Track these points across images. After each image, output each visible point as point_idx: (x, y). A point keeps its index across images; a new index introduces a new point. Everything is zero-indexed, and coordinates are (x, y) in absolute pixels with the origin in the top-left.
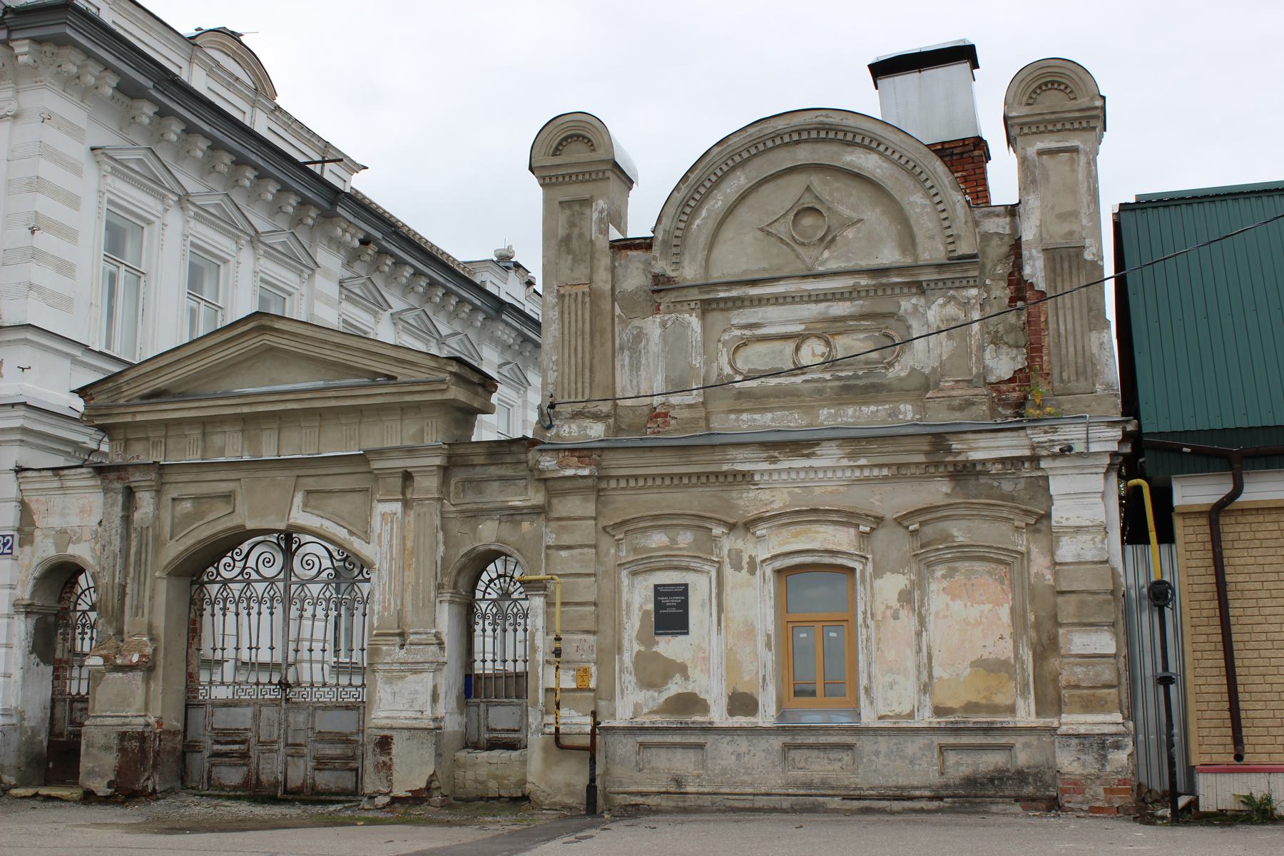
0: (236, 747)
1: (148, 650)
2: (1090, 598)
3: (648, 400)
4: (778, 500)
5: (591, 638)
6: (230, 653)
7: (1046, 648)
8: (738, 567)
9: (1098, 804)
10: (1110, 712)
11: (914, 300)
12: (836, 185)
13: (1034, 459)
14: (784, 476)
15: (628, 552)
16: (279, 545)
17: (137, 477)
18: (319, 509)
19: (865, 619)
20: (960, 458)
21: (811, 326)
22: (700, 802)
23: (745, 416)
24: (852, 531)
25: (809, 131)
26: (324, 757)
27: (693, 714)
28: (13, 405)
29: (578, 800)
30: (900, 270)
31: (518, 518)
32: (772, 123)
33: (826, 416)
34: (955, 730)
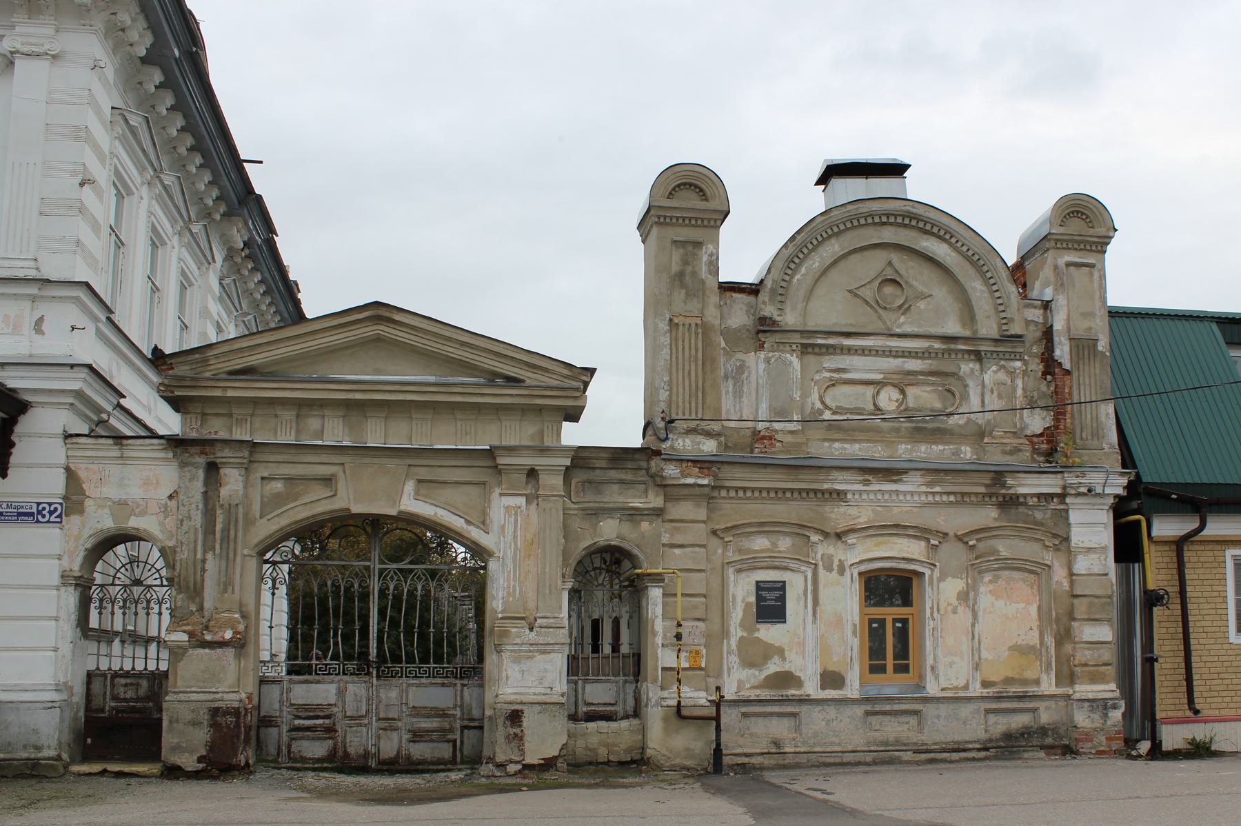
1: (241, 627)
2: (1096, 601)
3: (750, 424)
4: (863, 516)
7: (1064, 636)
8: (829, 569)
9: (1102, 749)
10: (1108, 683)
11: (971, 365)
12: (911, 264)
13: (1062, 497)
14: (872, 496)
17: (227, 452)
19: (932, 614)
20: (1011, 491)
22: (797, 760)
23: (837, 445)
24: (923, 543)
25: (896, 216)
27: (789, 688)
28: (72, 366)
29: (708, 762)
30: (965, 339)
31: (638, 518)
32: (868, 204)
33: (903, 450)
34: (998, 698)
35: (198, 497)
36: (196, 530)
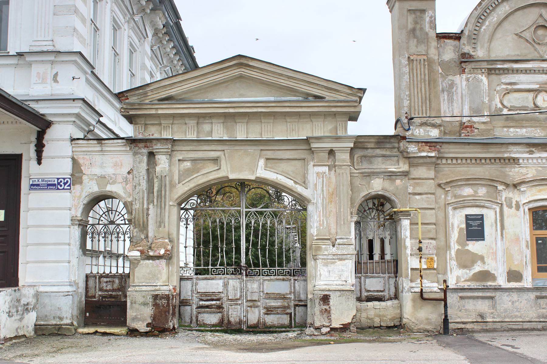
0: (214, 302)
1: (169, 247)
3: (458, 119)
4: (530, 173)
5: (433, 242)
8: (510, 206)
14: (535, 161)
15: (451, 197)
16: (237, 189)
17: (159, 146)
18: (274, 169)
21: (542, 86)
22: (495, 326)
23: (512, 130)
26: (271, 307)
27: (488, 281)
28: (74, 100)
31: (394, 177)
36: (143, 191)
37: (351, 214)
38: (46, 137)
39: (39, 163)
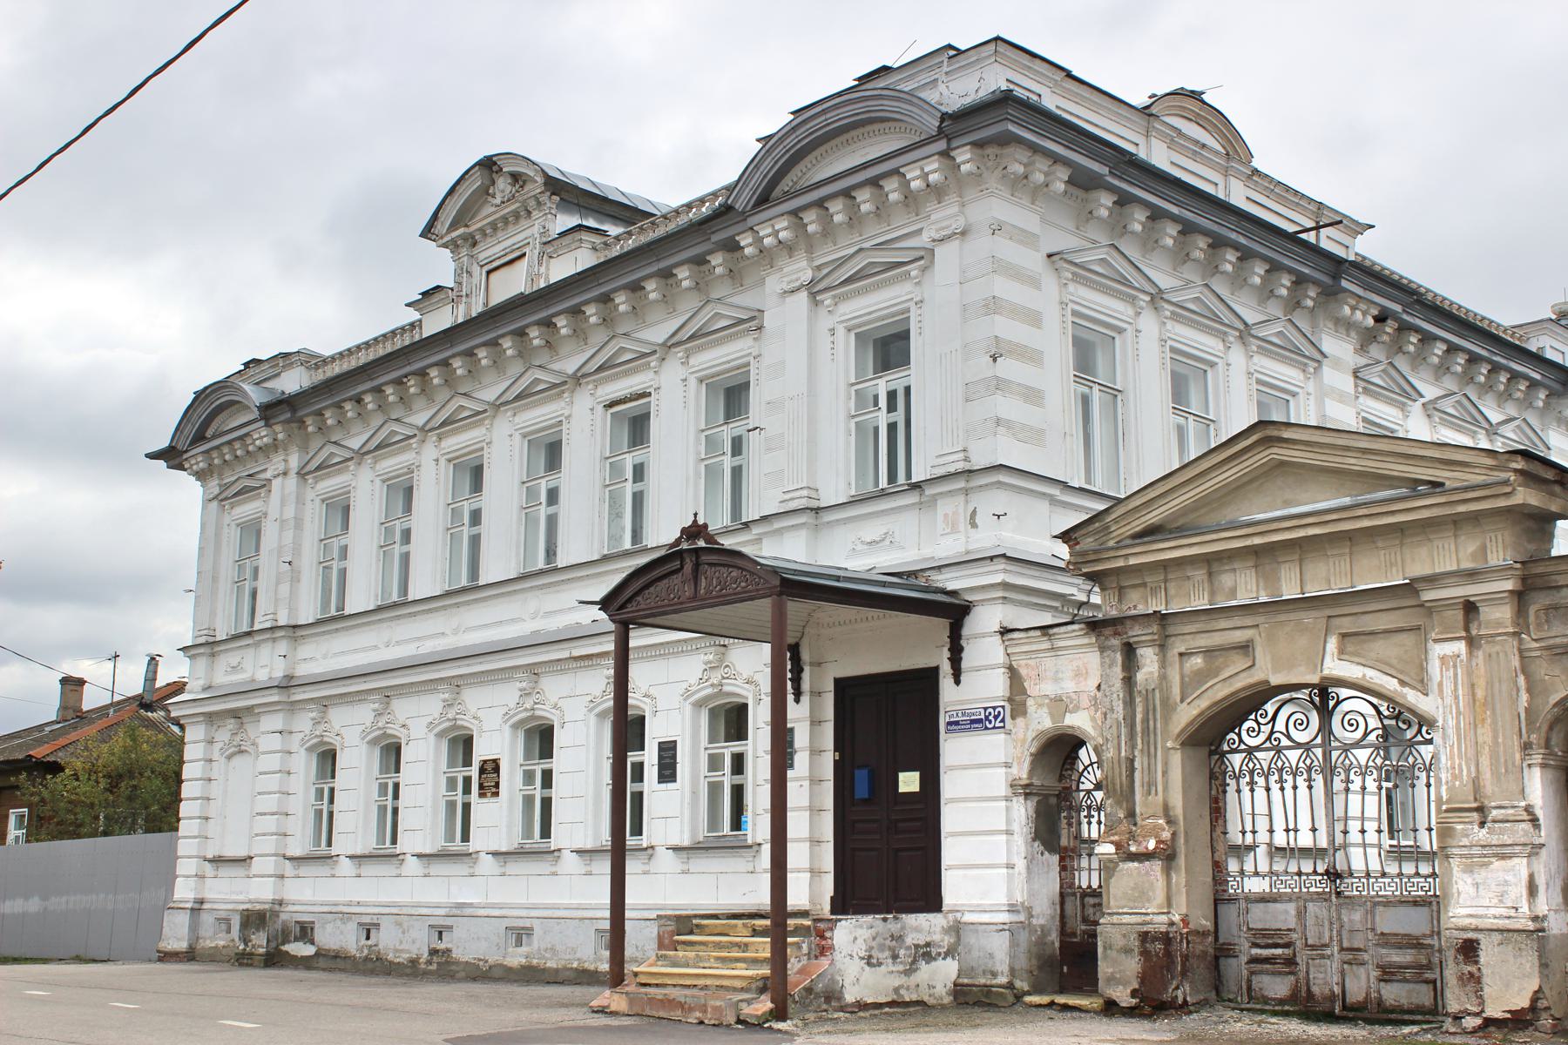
0: (1279, 951)
1: (1166, 835)
6: (1263, 837)
26: (1391, 965)
28: (992, 558)
35: (1118, 684)
36: (1119, 725)
37: (1526, 747)
38: (966, 632)
39: (957, 682)
